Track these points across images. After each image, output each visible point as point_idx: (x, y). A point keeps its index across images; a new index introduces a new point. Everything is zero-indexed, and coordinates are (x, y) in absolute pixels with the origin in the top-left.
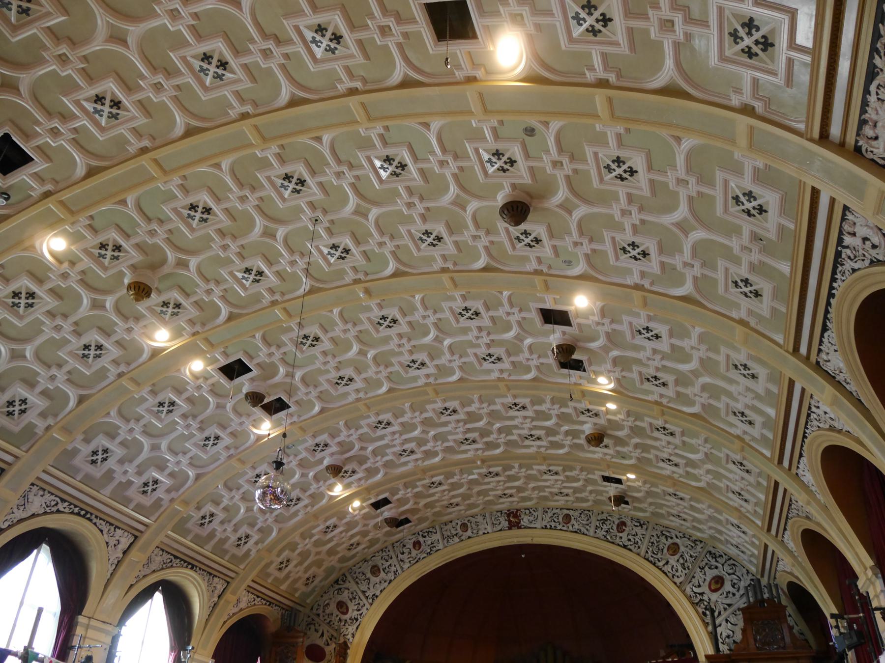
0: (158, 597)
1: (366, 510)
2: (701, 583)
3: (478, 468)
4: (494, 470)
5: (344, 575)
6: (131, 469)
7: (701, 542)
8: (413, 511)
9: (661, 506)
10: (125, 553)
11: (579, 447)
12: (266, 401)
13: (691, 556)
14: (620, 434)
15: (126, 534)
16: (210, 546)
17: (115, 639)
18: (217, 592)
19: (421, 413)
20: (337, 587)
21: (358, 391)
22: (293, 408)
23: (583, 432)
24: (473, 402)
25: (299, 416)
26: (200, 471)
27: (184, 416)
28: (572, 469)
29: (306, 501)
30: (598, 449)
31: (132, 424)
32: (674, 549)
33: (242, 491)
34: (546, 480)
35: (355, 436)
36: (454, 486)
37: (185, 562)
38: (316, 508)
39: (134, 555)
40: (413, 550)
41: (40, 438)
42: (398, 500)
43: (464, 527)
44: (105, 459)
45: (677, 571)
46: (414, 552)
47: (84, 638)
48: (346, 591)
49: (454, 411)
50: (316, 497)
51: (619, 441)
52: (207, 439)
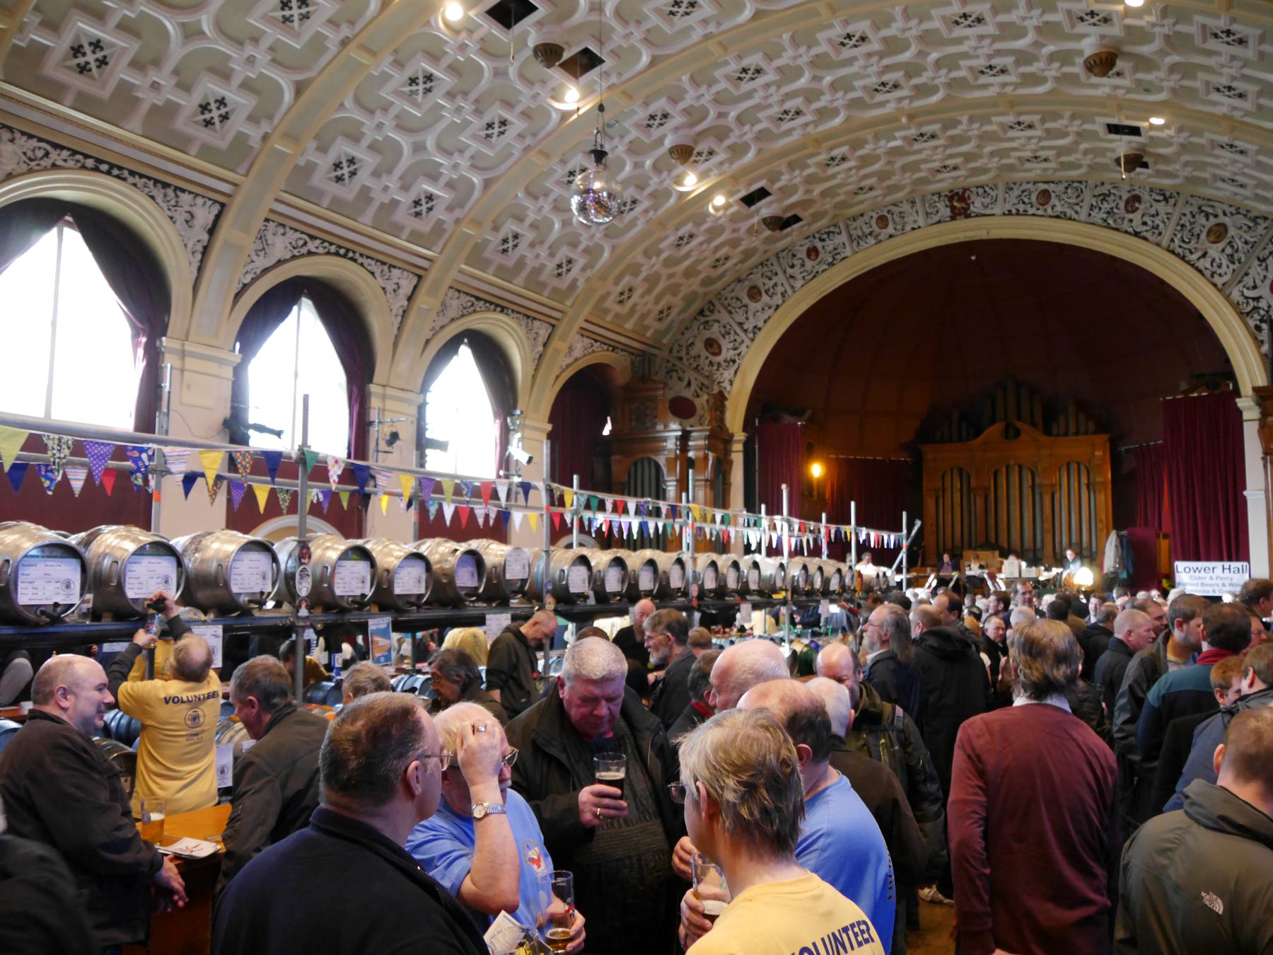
0: (465, 352)
1: (735, 209)
2: (1258, 283)
3: (902, 128)
4: (927, 129)
5: (711, 302)
6: (392, 182)
7: (1266, 219)
8: (805, 204)
9: (1203, 166)
10: (409, 299)
11: (1072, 79)
12: (566, 55)
13: (1246, 242)
14: (1145, 50)
15: (406, 274)
16: (521, 279)
17: (421, 408)
18: (541, 340)
19: (809, 47)
20: (703, 319)
21: (705, 22)
22: (609, 63)
23: (1080, 52)
24: (893, 19)
25: (620, 74)
26: (489, 175)
27: (450, 95)
28: (1056, 116)
29: (645, 204)
30: (1104, 80)
31: (379, 117)
32: (1218, 233)
33: (552, 197)
34: (1013, 139)
35: (708, 97)
36: (866, 161)
37: (491, 303)
38: (660, 212)
39: (422, 301)
40: (807, 260)
41: (258, 154)
42: (780, 189)
43: (882, 221)
44: (353, 174)
45: (1220, 266)
46: (809, 264)
47: (382, 411)
48: (716, 325)
49: (863, 39)
50: (660, 196)
51: (1144, 63)
52: (490, 126)
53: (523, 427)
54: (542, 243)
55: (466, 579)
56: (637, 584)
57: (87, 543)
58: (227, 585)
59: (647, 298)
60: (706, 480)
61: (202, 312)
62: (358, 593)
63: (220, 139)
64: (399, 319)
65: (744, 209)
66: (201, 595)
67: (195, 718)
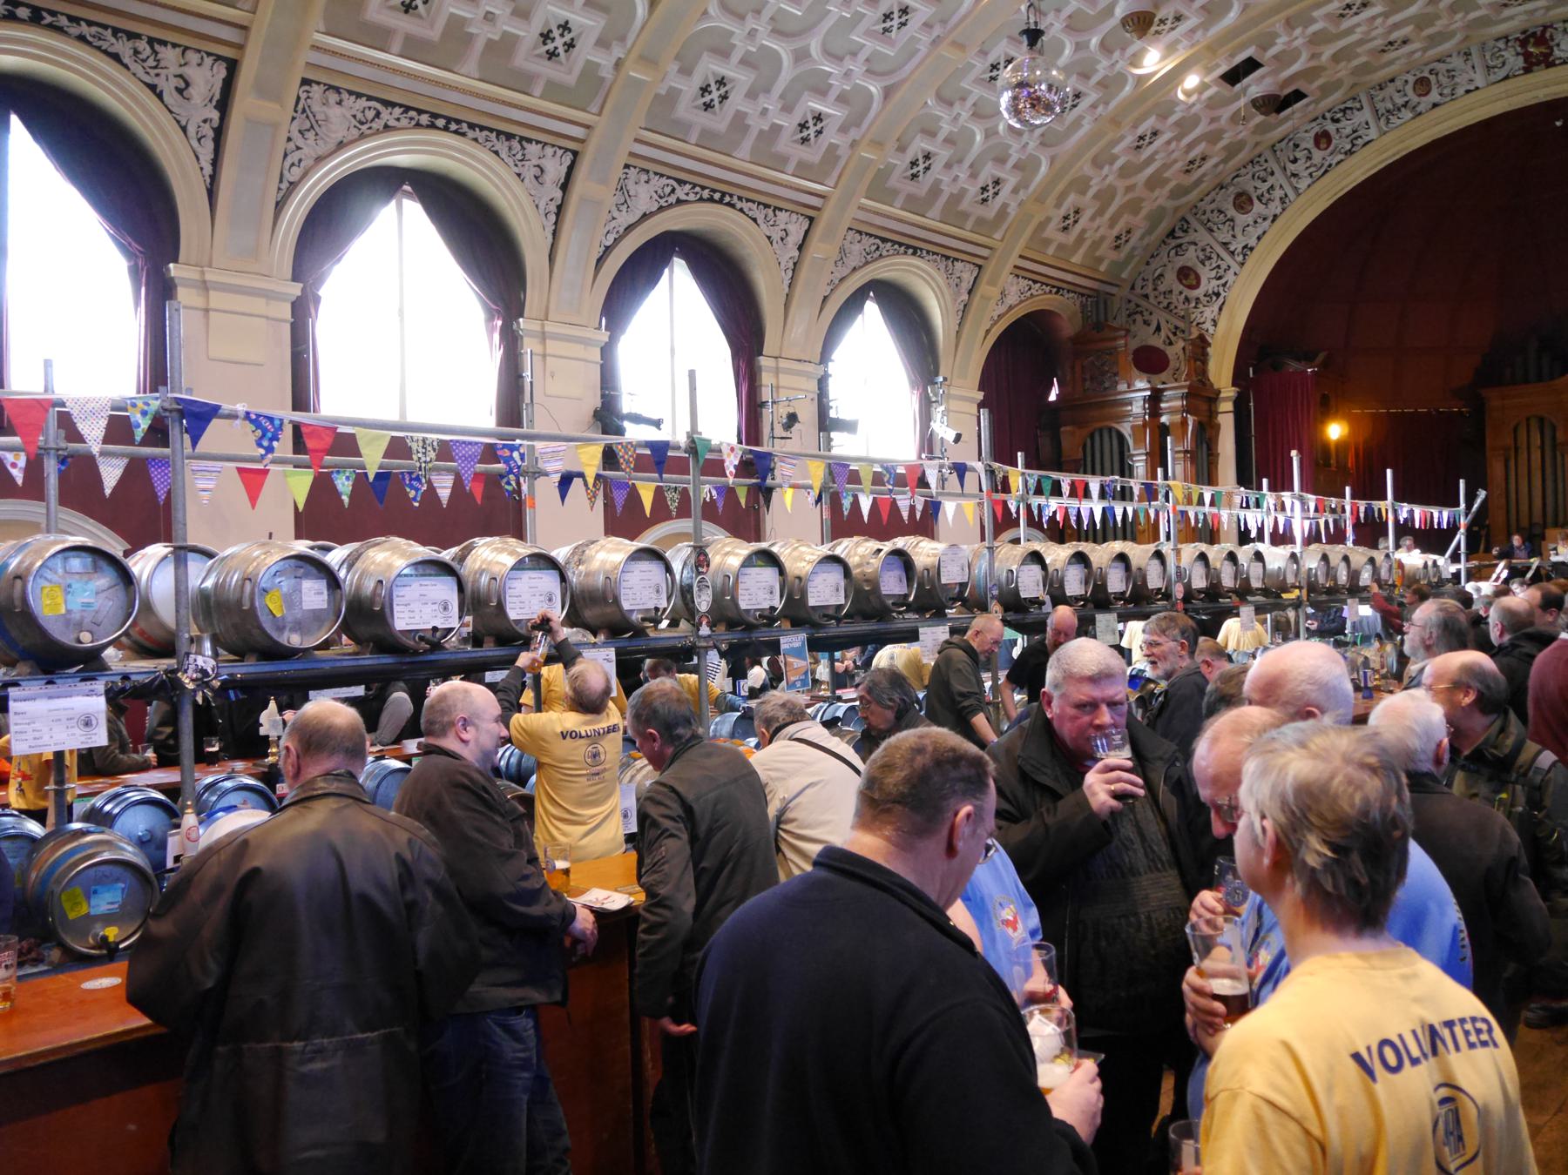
0: (871, 308)
5: (1184, 219)
6: (771, 103)
15: (794, 216)
17: (822, 382)
18: (965, 286)
20: (1174, 243)
37: (901, 245)
39: (817, 249)
44: (724, 97)
47: (776, 388)
48: (1192, 248)
53: (948, 397)
54: (960, 161)
55: (893, 585)
56: (1104, 586)
57: (461, 559)
58: (617, 601)
59: (1098, 221)
60: (1186, 452)
61: (564, 284)
62: (766, 605)
63: (566, 73)
64: (790, 273)
65: (1226, 90)
66: (589, 614)
67: (595, 756)
